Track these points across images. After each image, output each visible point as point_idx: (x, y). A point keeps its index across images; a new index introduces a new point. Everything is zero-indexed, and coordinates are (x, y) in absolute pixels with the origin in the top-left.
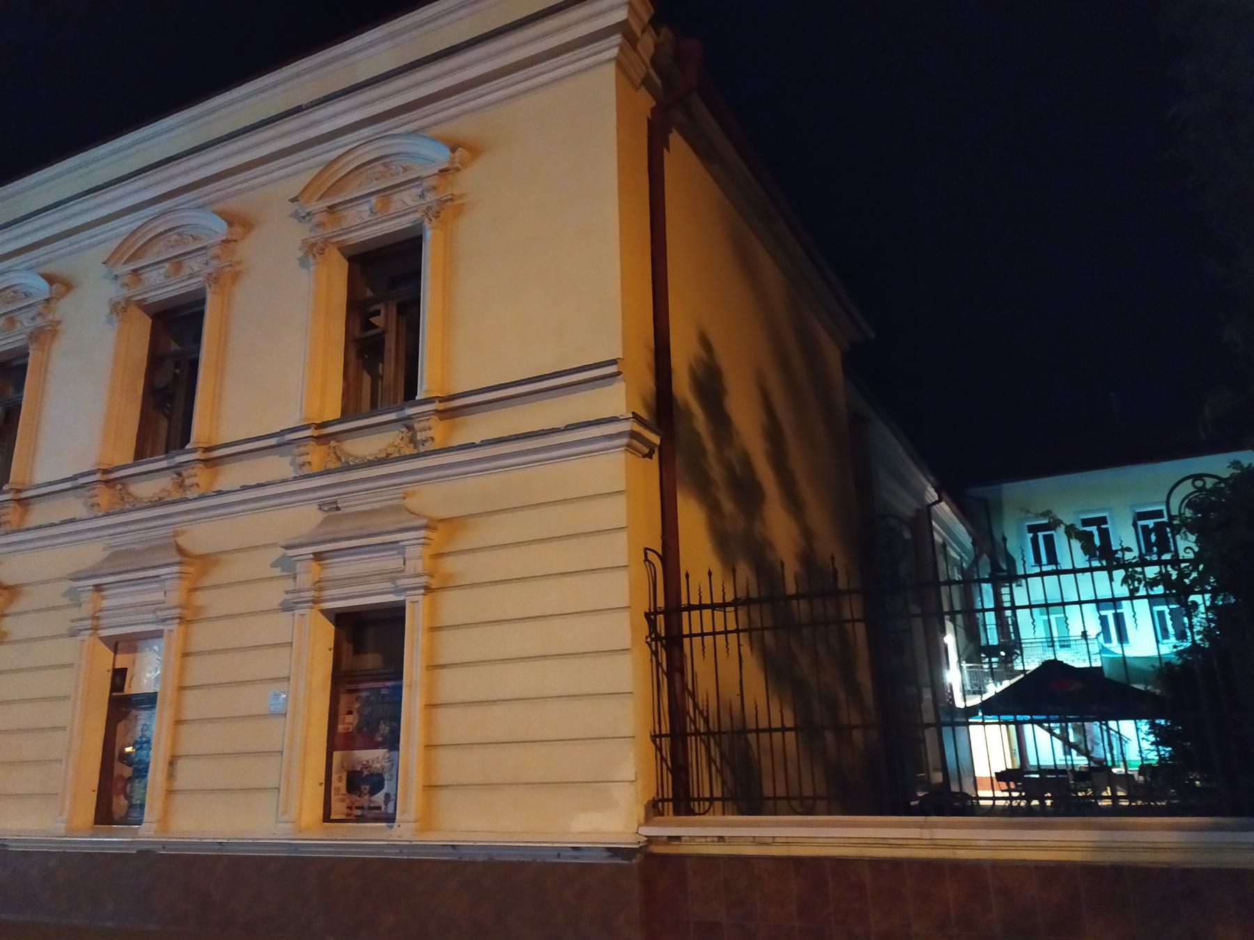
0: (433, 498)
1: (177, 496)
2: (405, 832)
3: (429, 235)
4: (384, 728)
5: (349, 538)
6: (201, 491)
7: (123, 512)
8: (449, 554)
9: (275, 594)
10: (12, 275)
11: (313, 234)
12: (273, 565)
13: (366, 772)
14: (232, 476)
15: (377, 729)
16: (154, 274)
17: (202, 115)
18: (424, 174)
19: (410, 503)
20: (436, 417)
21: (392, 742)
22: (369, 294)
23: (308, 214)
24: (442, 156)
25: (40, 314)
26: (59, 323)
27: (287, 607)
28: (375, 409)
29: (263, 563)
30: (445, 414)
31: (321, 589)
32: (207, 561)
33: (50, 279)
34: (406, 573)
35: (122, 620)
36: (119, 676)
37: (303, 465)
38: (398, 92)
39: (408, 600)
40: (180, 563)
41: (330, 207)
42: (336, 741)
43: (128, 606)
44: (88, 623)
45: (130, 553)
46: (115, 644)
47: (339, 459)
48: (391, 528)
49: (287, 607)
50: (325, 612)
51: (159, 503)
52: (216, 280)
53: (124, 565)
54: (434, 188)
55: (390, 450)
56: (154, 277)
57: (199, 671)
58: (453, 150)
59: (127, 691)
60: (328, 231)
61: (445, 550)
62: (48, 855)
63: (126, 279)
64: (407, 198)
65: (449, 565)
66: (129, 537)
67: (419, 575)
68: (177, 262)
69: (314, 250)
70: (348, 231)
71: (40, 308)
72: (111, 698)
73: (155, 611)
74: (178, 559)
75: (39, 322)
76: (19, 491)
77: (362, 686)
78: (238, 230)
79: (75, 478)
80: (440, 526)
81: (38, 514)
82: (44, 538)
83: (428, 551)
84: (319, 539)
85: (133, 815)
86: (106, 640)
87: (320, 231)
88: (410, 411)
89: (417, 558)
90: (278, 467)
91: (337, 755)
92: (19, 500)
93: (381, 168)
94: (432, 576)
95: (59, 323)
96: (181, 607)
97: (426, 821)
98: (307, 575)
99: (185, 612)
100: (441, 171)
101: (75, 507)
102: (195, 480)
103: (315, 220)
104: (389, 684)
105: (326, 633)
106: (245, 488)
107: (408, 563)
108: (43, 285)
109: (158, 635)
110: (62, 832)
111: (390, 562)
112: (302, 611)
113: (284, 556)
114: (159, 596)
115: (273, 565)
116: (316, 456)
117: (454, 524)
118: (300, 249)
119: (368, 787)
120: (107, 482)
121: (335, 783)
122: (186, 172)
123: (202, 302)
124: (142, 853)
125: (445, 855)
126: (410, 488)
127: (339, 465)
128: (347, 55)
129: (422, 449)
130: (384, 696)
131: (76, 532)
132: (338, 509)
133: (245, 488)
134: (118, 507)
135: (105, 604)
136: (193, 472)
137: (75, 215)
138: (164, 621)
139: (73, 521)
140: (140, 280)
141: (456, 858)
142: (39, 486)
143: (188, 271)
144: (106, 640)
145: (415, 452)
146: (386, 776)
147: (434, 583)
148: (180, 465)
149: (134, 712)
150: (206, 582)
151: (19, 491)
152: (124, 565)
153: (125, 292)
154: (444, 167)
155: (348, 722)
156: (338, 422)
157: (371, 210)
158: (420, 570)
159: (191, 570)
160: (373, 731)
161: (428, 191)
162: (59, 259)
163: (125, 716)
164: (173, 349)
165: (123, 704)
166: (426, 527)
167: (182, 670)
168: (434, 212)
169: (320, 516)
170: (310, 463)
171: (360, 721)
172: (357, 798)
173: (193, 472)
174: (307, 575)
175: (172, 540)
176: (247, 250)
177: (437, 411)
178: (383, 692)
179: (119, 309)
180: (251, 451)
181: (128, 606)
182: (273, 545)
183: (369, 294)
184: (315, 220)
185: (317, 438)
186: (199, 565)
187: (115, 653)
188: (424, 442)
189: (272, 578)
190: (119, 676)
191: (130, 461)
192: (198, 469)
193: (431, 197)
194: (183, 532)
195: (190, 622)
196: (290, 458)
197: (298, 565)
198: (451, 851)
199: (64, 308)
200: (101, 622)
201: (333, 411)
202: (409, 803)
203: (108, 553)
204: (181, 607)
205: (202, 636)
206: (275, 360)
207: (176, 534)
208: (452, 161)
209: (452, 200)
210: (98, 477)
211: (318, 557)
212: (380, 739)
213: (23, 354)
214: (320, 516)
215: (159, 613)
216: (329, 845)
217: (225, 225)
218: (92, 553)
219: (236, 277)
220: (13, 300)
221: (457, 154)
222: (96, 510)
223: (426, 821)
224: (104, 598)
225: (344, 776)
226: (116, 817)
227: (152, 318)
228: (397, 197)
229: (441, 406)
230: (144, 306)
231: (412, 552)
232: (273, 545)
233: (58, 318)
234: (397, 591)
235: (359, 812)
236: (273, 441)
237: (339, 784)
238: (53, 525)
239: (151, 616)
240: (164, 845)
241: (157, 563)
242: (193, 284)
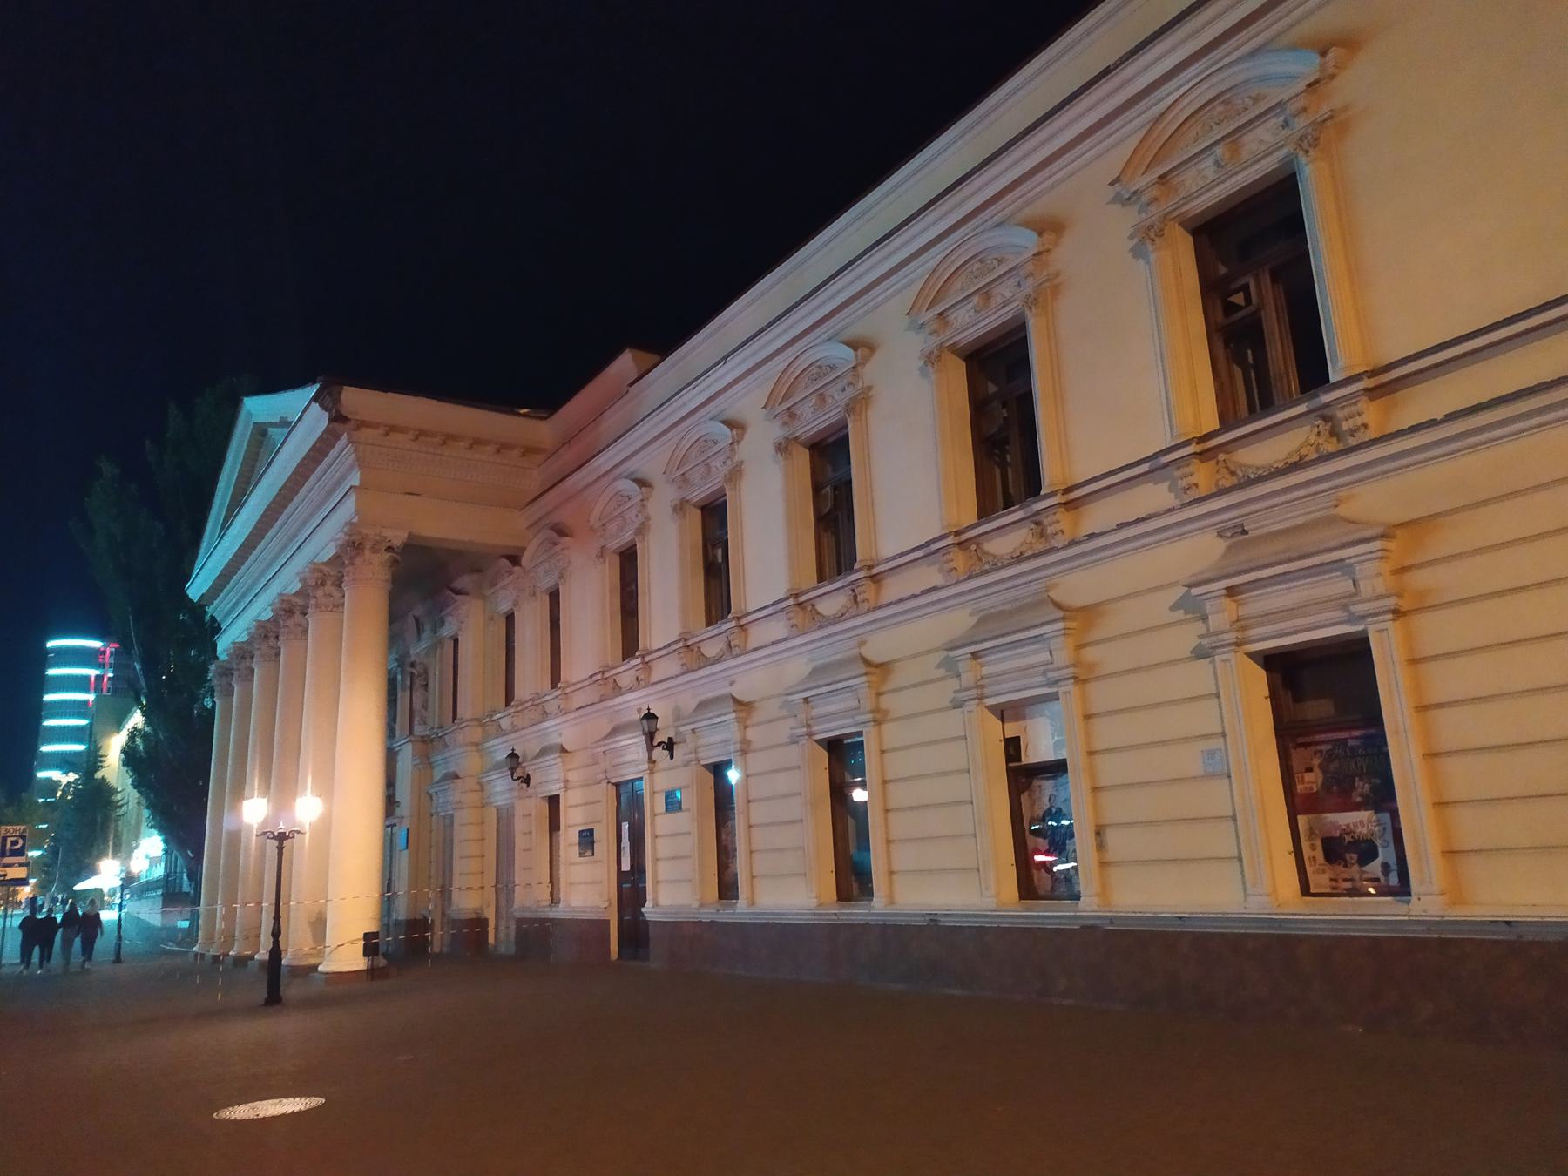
0: (1376, 500)
1: (1039, 547)
2: (879, 905)
3: (1032, 324)
4: (1363, 787)
5: (1272, 565)
6: (872, 604)
7: (986, 572)
8: (1420, 566)
9: (1188, 636)
10: (811, 352)
11: (1143, 216)
12: (1174, 608)
13: (1348, 838)
14: (1099, 516)
15: (1353, 787)
16: (963, 311)
17: (923, 167)
18: (1284, 96)
19: (1343, 511)
20: (1364, 398)
21: (1383, 798)
22: (1223, 270)
23: (1135, 193)
24: (1306, 66)
25: (850, 384)
26: (870, 388)
27: (957, 705)
28: (1008, 503)
29: (1160, 607)
30: (1069, 505)
31: (1244, 629)
32: (1088, 614)
33: (854, 345)
34: (1056, 665)
35: (1005, 687)
36: (1013, 747)
37: (1186, 490)
38: (1024, 157)
39: (1061, 690)
40: (1064, 619)
41: (1161, 177)
42: (1296, 804)
43: (1013, 671)
44: (974, 692)
45: (1000, 615)
46: (1001, 713)
47: (1233, 473)
48: (1333, 544)
49: (1200, 654)
50: (1252, 656)
51: (1019, 559)
52: (1315, 143)
53: (993, 629)
54: (1304, 110)
55: (1303, 452)
56: (962, 316)
57: (1108, 733)
58: (1323, 54)
59: (1024, 761)
60: (943, 337)
61: (1407, 563)
62: (981, 931)
63: (934, 326)
64: (1265, 134)
65: (1420, 579)
66: (995, 600)
67: (1382, 597)
68: (985, 293)
69: (1148, 235)
70: (1190, 198)
71: (1030, 267)
72: (1009, 770)
73: (1044, 673)
74: (1060, 614)
75: (851, 392)
76: (870, 568)
77: (1318, 738)
78: (1048, 237)
79: (928, 544)
80: (1399, 532)
81: (894, 588)
82: (906, 612)
83: (1386, 567)
84: (1231, 570)
85: (866, 891)
86: (991, 708)
87: (1153, 209)
88: (1326, 398)
89: (1374, 579)
90: (1155, 496)
91: (1302, 820)
92: (871, 577)
93: (978, 265)
94: (1399, 595)
95: (870, 388)
96: (1074, 665)
97: (1455, 892)
98: (1222, 615)
99: (1400, 602)
100: (1309, 86)
101: (930, 575)
102: (1057, 527)
103: (1145, 199)
104: (1356, 733)
105: (1259, 679)
106: (1121, 526)
107: (1362, 584)
108: (848, 352)
109: (1054, 697)
110: (993, 906)
111: (1342, 585)
112: (1224, 657)
113: (947, 657)
114: (1045, 657)
115: (1174, 608)
116: (1202, 475)
117: (1416, 527)
118: (1131, 237)
119: (1355, 856)
120: (959, 544)
121: (1307, 852)
122: (762, 348)
123: (1023, 327)
124: (1084, 928)
125: (1494, 933)
126: (1343, 493)
127: (1234, 481)
128: (727, 322)
129: (1352, 442)
130: (1353, 749)
131: (940, 601)
132: (1245, 532)
133: (1121, 526)
134: (977, 569)
135: (986, 671)
136: (1054, 518)
137: (838, 292)
138: (1056, 682)
139: (935, 589)
140: (946, 324)
141: (1512, 937)
142: (889, 559)
143: (999, 300)
144: (991, 708)
145: (1341, 447)
146: (1378, 842)
147: (1405, 605)
148: (853, 582)
149: (1036, 783)
150: (1096, 635)
151: (870, 568)
152: (993, 629)
153: (934, 341)
154: (1312, 79)
155: (1311, 781)
156: (814, 589)
157: (1217, 163)
158: (1381, 589)
159: (1073, 624)
160: (1347, 791)
161: (1295, 116)
162: (857, 323)
163: (1028, 787)
164: (1000, 394)
165: (1024, 776)
166: (1382, 536)
167: (1088, 735)
168: (1309, 142)
169: (1221, 545)
170: (1365, 426)
171: (1325, 779)
172: (1341, 868)
173: (1054, 518)
174: (1222, 615)
175: (855, 651)
176: (1066, 255)
177: (1366, 390)
178: (1351, 743)
179: (783, 448)
180: (1465, 355)
181: (1013, 671)
182: (1176, 583)
183: (1223, 270)
184: (1145, 199)
185: (1200, 454)
186: (879, 669)
187: (1002, 720)
188: (1352, 433)
189: (1175, 623)
190: (1013, 747)
191: (814, 582)
192: (1061, 514)
193: (1300, 123)
194: (1056, 585)
195: (1085, 681)
196: (1167, 484)
197: (1208, 604)
198: (1505, 927)
199: (870, 372)
200: (986, 691)
201: (1212, 423)
202: (1426, 870)
203: (976, 619)
204: (872, 712)
205: (1102, 695)
206: (1129, 378)
207: (862, 643)
208: (1323, 67)
209: (1331, 117)
210: (950, 540)
211: (1231, 592)
212: (1359, 799)
213: (721, 493)
214: (1221, 545)
215: (1050, 675)
216: (1303, 921)
217: (1034, 236)
218: (960, 620)
219: (1056, 290)
220: (819, 377)
221: (1330, 55)
222: (954, 576)
223: (1455, 892)
224: (982, 665)
225: (1318, 843)
226: (1041, 892)
227: (965, 360)
228: (1247, 138)
229: (1064, 499)
230: (955, 350)
231: (1365, 570)
232: (1176, 583)
233: (867, 384)
234: (1352, 620)
235: (1348, 885)
236: (1145, 467)
237: (1313, 852)
238: (914, 596)
239: (1041, 679)
240: (1112, 920)
241: (1038, 621)
242: (1268, 165)
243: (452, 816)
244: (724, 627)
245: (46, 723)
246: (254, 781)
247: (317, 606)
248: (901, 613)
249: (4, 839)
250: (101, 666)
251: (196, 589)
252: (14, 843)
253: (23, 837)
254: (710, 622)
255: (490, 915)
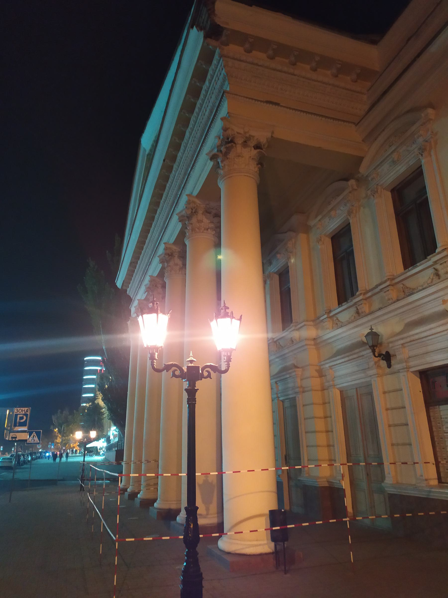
120: (366, 299)
148: (355, 303)
210: (388, 283)
243: (294, 399)
244: (354, 301)
245: (85, 377)
246: (292, 257)
247: (193, 230)
248: (384, 315)
249: (16, 415)
250: (101, 366)
251: (119, 284)
252: (21, 418)
253: (26, 415)
254: (340, 303)
255: (345, 485)
